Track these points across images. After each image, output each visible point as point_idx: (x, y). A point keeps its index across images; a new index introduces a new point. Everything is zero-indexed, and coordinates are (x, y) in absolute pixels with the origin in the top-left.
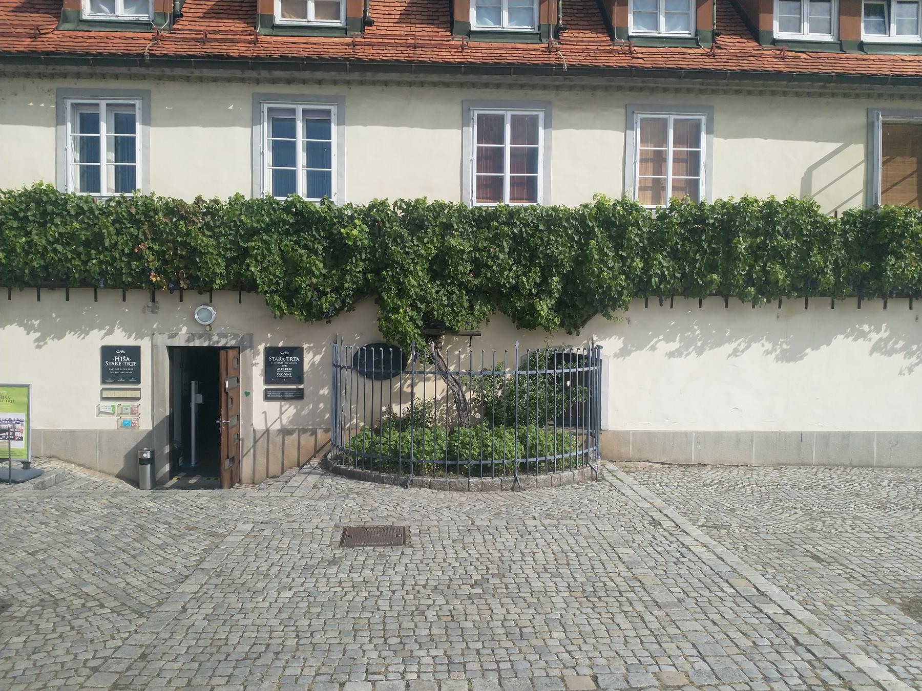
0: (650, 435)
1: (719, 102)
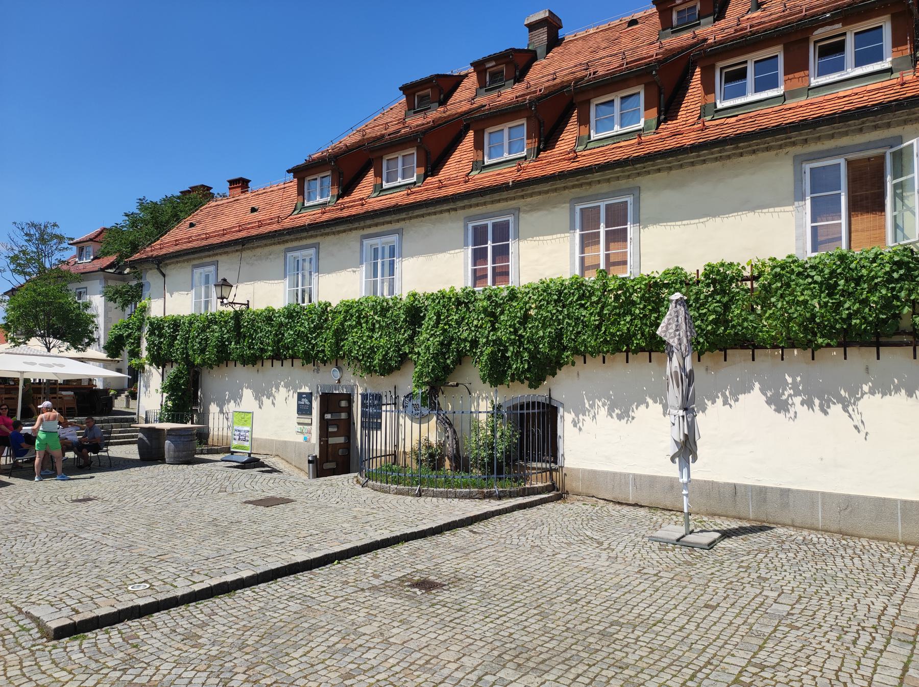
0: (594, 473)
1: (643, 181)
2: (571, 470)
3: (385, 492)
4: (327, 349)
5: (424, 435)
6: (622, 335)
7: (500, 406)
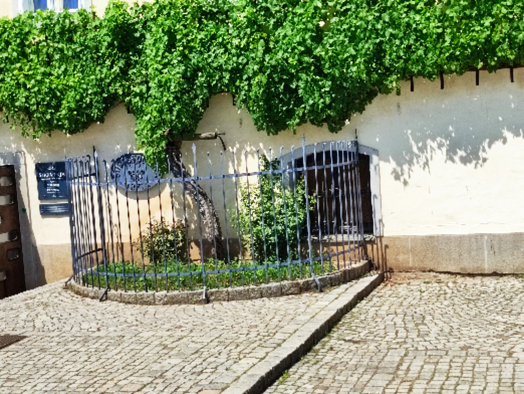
2: (394, 239)
3: (149, 303)
4: (118, 84)
5: (156, 216)
6: (476, 46)
7: (275, 164)
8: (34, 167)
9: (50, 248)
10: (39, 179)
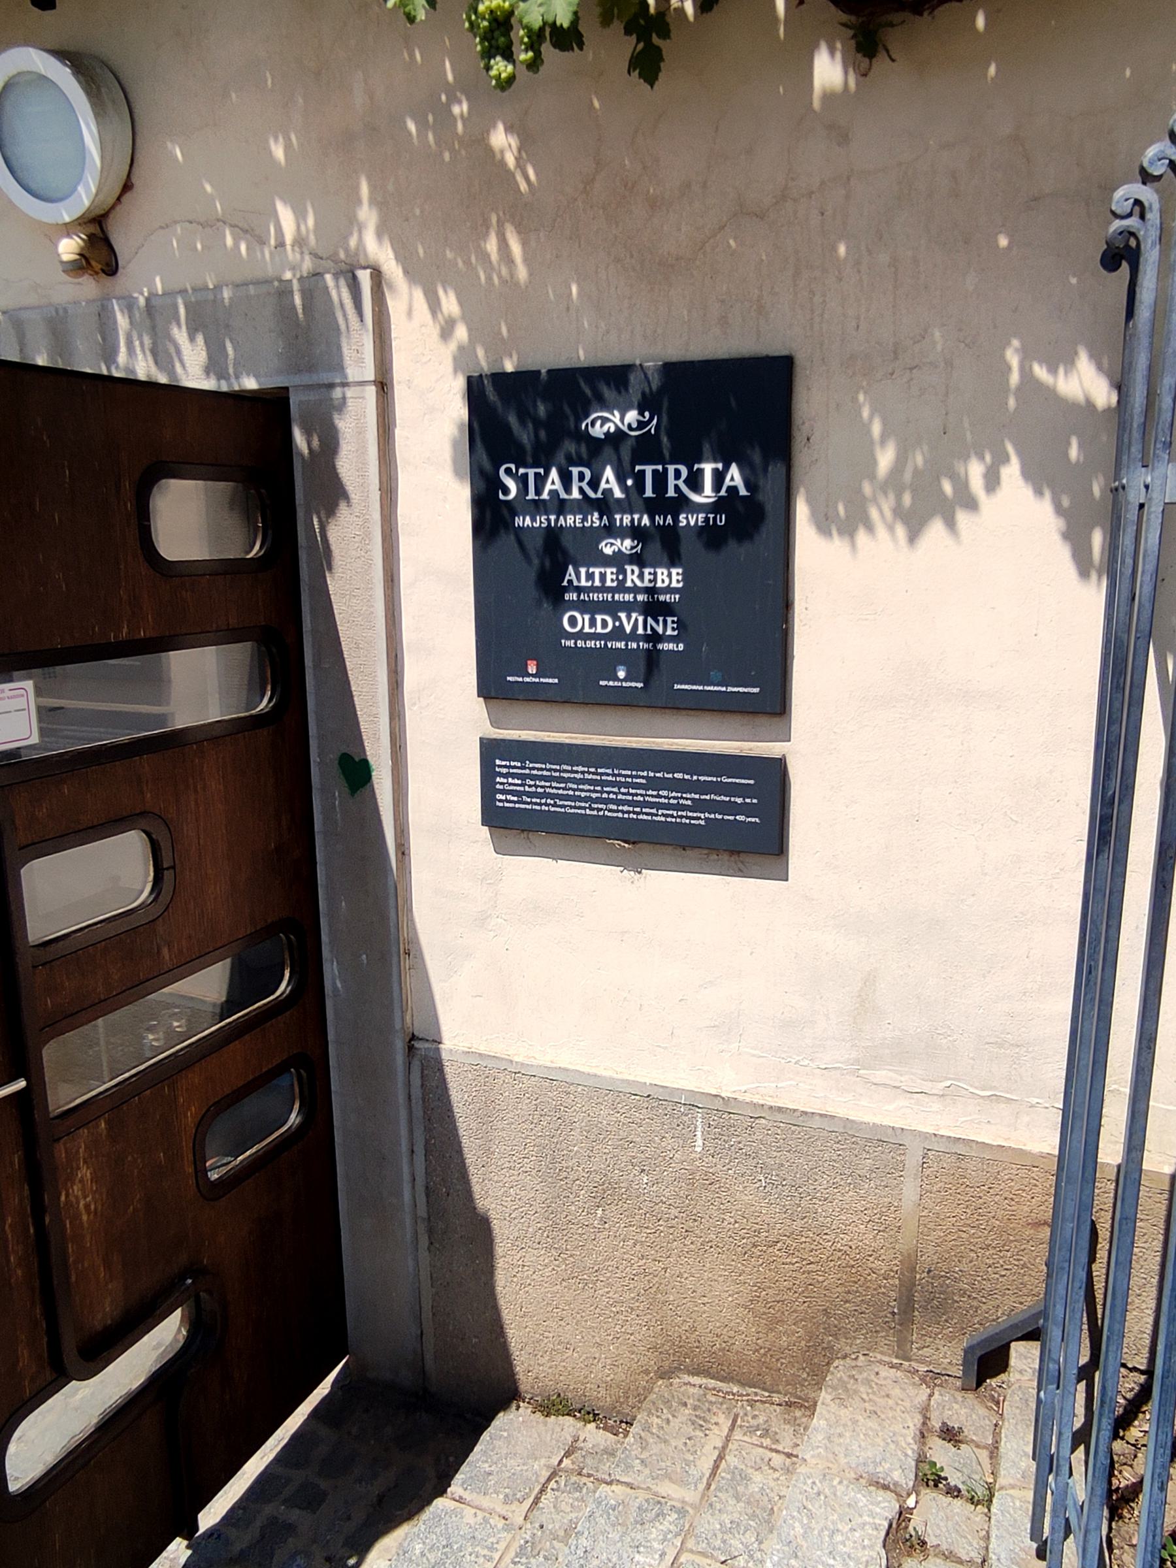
8: (459, 410)
9: (557, 1097)
10: (490, 517)
